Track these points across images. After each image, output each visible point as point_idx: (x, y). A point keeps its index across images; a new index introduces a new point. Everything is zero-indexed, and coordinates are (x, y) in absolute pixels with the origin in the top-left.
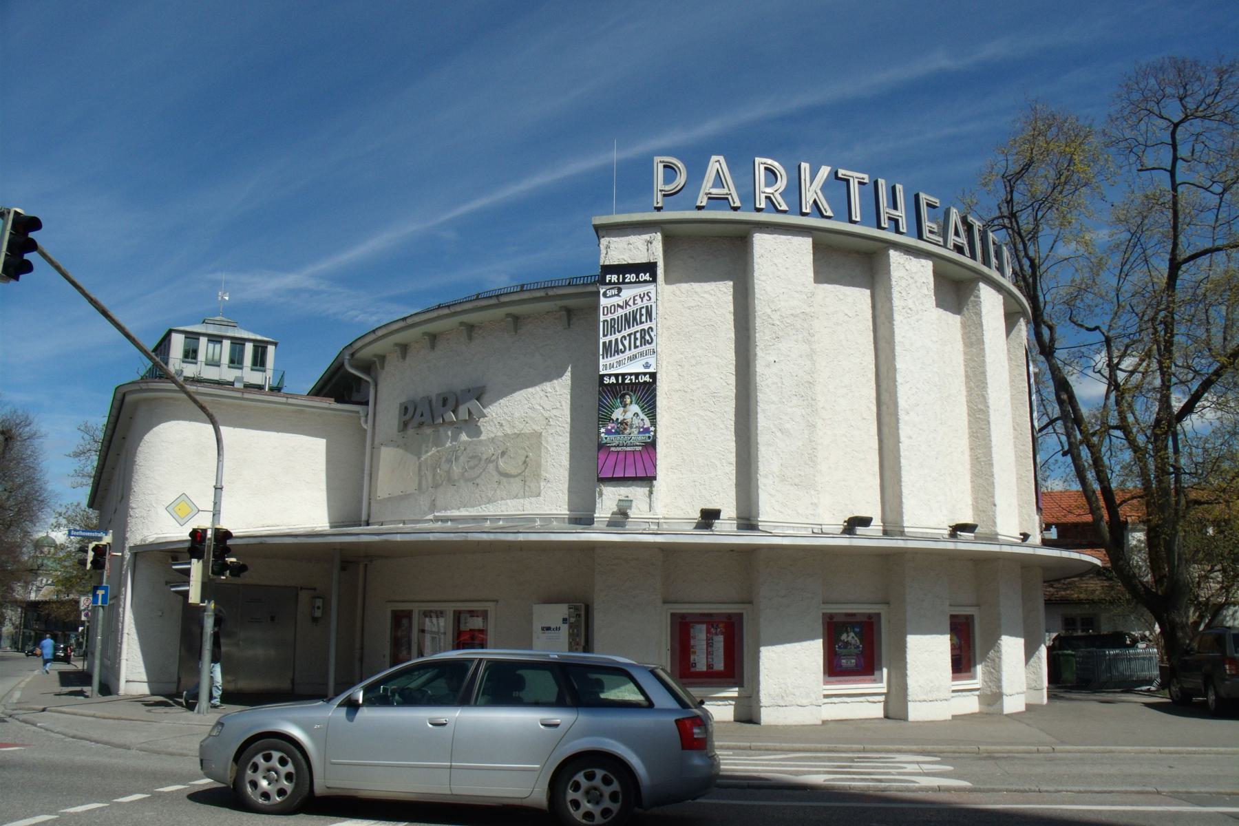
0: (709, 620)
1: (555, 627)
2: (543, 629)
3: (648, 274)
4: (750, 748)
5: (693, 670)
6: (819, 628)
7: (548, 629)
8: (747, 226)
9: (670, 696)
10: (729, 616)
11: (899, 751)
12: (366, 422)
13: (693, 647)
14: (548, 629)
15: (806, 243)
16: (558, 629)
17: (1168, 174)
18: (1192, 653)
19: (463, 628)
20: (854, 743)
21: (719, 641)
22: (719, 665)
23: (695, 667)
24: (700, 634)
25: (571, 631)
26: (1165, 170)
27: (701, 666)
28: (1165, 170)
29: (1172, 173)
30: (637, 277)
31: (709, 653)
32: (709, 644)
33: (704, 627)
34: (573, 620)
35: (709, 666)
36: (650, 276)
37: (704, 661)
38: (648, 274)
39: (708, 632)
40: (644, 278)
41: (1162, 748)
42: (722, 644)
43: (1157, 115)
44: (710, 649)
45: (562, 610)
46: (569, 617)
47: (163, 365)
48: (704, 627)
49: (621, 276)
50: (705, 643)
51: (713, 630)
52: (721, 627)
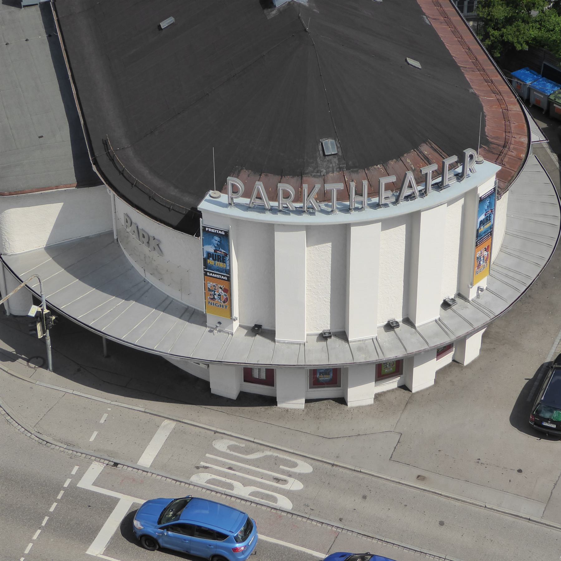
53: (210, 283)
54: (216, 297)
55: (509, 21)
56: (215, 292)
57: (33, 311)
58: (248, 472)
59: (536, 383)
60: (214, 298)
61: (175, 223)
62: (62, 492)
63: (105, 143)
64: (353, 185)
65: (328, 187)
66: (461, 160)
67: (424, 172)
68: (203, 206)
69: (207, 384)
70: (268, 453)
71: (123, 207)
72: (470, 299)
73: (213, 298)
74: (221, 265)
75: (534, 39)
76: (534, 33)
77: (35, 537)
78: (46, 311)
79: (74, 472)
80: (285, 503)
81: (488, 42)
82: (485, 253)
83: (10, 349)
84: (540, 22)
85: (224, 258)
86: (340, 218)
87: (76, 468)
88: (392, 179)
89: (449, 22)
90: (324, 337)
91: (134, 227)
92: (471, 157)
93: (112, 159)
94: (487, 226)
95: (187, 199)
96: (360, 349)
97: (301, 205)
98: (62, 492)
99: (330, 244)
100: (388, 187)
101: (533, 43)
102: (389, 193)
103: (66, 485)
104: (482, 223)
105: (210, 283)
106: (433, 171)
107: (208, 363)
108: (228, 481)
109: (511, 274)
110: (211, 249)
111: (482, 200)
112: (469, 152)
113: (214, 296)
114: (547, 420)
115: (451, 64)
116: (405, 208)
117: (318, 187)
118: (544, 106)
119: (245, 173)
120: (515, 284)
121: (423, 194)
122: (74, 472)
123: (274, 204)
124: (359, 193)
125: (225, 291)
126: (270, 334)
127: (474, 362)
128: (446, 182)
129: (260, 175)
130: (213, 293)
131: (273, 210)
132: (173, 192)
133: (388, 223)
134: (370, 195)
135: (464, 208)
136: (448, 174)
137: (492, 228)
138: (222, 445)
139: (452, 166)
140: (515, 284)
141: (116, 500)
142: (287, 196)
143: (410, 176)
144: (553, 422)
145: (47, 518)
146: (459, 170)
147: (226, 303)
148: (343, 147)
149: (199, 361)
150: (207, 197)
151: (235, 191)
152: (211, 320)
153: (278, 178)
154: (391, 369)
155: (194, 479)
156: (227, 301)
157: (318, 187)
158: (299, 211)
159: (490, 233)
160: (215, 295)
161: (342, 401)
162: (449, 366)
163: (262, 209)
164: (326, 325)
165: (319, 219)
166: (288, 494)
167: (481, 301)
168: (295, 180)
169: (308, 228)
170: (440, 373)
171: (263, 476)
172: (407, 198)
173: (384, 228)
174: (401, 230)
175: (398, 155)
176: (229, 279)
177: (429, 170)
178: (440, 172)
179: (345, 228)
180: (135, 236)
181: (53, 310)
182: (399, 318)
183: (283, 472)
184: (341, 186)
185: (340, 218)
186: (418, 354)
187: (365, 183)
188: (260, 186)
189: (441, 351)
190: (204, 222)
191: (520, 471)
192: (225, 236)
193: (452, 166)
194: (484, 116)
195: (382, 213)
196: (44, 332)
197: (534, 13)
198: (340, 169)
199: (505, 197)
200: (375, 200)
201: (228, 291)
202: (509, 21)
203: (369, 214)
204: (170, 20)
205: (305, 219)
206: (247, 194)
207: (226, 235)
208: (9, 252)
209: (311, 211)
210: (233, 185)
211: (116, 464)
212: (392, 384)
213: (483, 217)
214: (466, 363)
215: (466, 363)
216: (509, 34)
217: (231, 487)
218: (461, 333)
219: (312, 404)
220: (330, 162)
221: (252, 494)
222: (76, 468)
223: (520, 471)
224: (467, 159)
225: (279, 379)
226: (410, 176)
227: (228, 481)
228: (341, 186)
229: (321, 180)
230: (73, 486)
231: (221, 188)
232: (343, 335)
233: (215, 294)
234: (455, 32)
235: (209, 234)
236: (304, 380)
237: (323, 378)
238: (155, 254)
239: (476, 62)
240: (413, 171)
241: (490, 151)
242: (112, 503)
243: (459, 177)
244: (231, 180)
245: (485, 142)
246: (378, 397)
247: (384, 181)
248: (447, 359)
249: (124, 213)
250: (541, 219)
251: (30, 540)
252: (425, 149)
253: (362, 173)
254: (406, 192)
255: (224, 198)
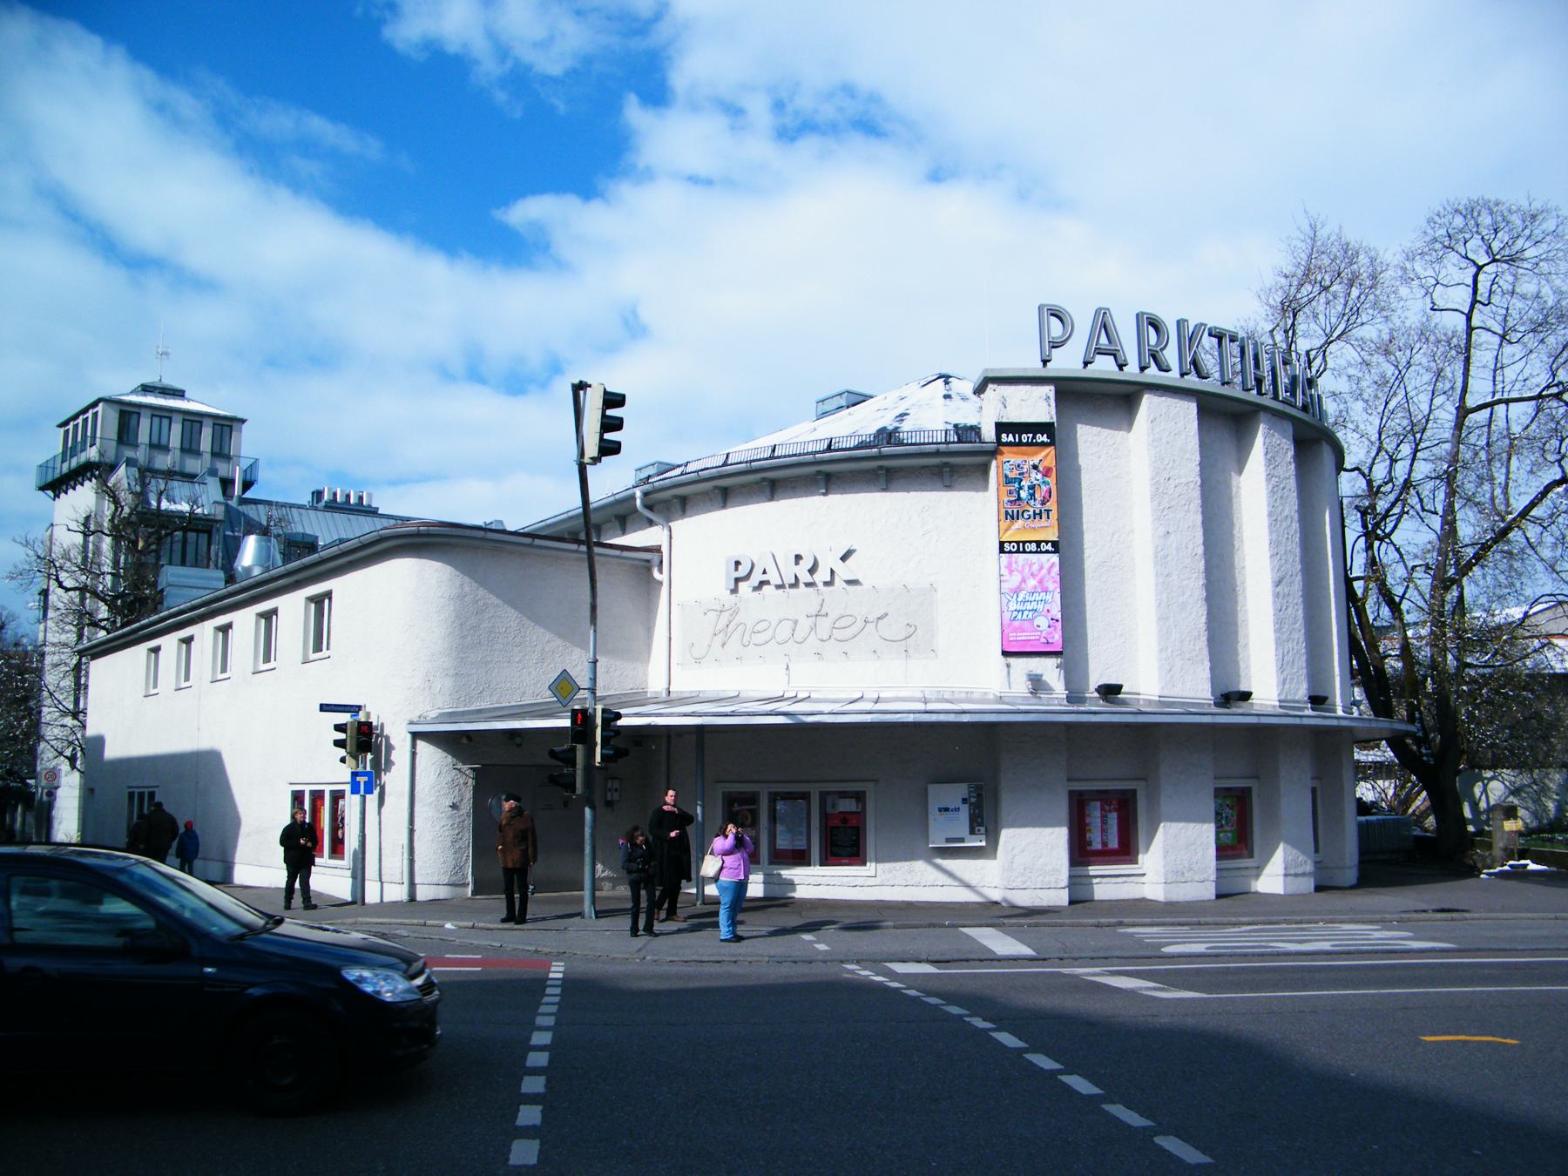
0: (1103, 796)
1: (953, 807)
2: (940, 810)
3: (1045, 435)
4: (1199, 924)
5: (1088, 848)
6: (1210, 806)
7: (946, 810)
8: (1135, 387)
9: (1421, 886)
10: (1124, 792)
11: (1342, 922)
12: (661, 571)
13: (1088, 825)
14: (946, 810)
15: (1191, 407)
16: (957, 810)
17: (1464, 317)
18: (1374, 810)
19: (829, 810)
20: (1243, 916)
21: (1113, 818)
22: (1114, 844)
23: (1091, 845)
24: (1094, 814)
25: (972, 811)
26: (1463, 313)
27: (1097, 845)
28: (1463, 313)
29: (1469, 318)
30: (1034, 437)
31: (1104, 831)
32: (1104, 822)
33: (1098, 804)
34: (973, 800)
35: (1104, 844)
36: (1048, 438)
37: (1099, 839)
38: (1045, 435)
39: (1102, 809)
40: (1042, 439)
41: (1558, 915)
42: (1115, 822)
43: (1461, 255)
44: (1104, 827)
45: (962, 790)
46: (970, 797)
47: (88, 445)
48: (1098, 804)
49: (1017, 435)
50: (1099, 820)
51: (1107, 808)
52: (1115, 805)
53: (1008, 462)
54: (1024, 494)
56: (1022, 480)
60: (1019, 498)
73: (1015, 500)
99: (1079, 426)
101: (1474, 709)
105: (1008, 462)
106: (321, 651)
113: (1019, 495)
130: (1016, 485)
147: (1048, 504)
154: (1417, 568)
156: (1050, 497)
160: (1021, 491)
233: (1021, 488)
249: (590, 386)
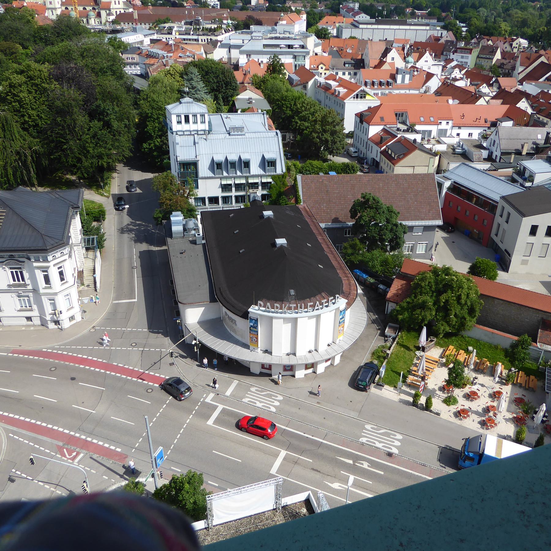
55: (352, 254)
57: (194, 342)
58: (260, 398)
59: (358, 372)
61: (240, 315)
62: (200, 403)
63: (220, 288)
64: (299, 305)
65: (291, 305)
66: (335, 298)
67: (322, 301)
68: (250, 310)
69: (249, 369)
70: (268, 392)
71: (224, 309)
72: (337, 343)
74: (255, 329)
75: (360, 260)
76: (360, 258)
77: (190, 417)
78: (198, 343)
79: (204, 396)
80: (273, 409)
81: (346, 260)
82: (342, 328)
83: (185, 355)
84: (363, 255)
85: (256, 327)
86: (294, 315)
87: (205, 395)
88: (312, 304)
89: (332, 254)
90: (288, 355)
91: (228, 316)
92: (338, 297)
93: (222, 294)
94: (343, 319)
95: (245, 307)
96: (300, 359)
97: (282, 311)
98: (200, 403)
100: (310, 306)
102: (311, 308)
103: (201, 400)
104: (341, 319)
107: (250, 362)
108: (255, 401)
109: (350, 336)
110: (252, 324)
111: (341, 312)
112: (337, 296)
114: (360, 385)
115: (333, 267)
116: (316, 313)
117: (287, 305)
118: (363, 281)
119: (264, 300)
120: (351, 339)
121: (322, 309)
122: (204, 396)
123: (273, 310)
124: (301, 308)
125: (256, 338)
126: (271, 353)
127: (338, 365)
128: (329, 305)
129: (41, 132)
131: (272, 312)
132: (241, 305)
133: (310, 317)
134: (304, 308)
135: (335, 313)
136: (330, 303)
137: (344, 320)
138: (253, 389)
139: (331, 300)
140: (351, 339)
141: (217, 407)
142: (277, 308)
143: (318, 303)
144: (362, 386)
145: (194, 411)
146: (334, 301)
148: (296, 292)
149: (247, 361)
150: (251, 307)
151: (261, 305)
152: (251, 348)
153: (275, 302)
154: (310, 366)
155: (243, 400)
157: (287, 305)
158: (281, 313)
159: (344, 321)
161: (294, 376)
162: (329, 366)
163: (269, 312)
164: (288, 351)
165: (287, 315)
166: (274, 406)
167: (340, 344)
168: (280, 303)
169: (284, 319)
170: (326, 368)
171: (266, 400)
172: (316, 310)
173: (308, 319)
174: (314, 320)
175: (314, 296)
176: (257, 334)
177: (324, 301)
178: (328, 302)
179: (296, 319)
180: (228, 319)
181: (200, 342)
182: (313, 349)
183: (273, 399)
184: (295, 305)
185: (294, 315)
186: (319, 361)
187: (303, 305)
188: (268, 304)
189: (327, 361)
190: (250, 315)
191: (351, 402)
192: (257, 320)
193: (331, 300)
194: (343, 284)
195: (308, 314)
196: (197, 349)
197: (361, 252)
198: (295, 300)
199: (349, 310)
200: (306, 310)
201: (257, 338)
202: (352, 254)
203: (304, 314)
204: (243, 250)
205: (283, 315)
206: (264, 307)
207: (257, 319)
208: (187, 323)
209: (285, 313)
210: (260, 304)
211: (218, 394)
212: (310, 371)
213: (341, 317)
214: (335, 364)
215: (335, 364)
216: (352, 258)
217: (256, 403)
218: (333, 355)
219: (284, 377)
220: (292, 297)
221: (263, 406)
222: (205, 395)
223: (351, 402)
224: (337, 298)
225: (273, 368)
226: (318, 303)
227: (255, 401)
228: (295, 305)
229: (289, 303)
230: (204, 401)
231: (256, 304)
232: (294, 354)
234: (335, 257)
235: (251, 320)
236: (281, 370)
237: (308, 367)
238: (234, 325)
239: (341, 267)
240: (319, 301)
241: (344, 296)
242: (216, 407)
243: (334, 303)
244: (259, 302)
245: (343, 292)
246: (305, 375)
247: (309, 304)
248: (329, 363)
250: (361, 318)
251: (188, 418)
252: (323, 294)
253: (302, 301)
254: (316, 308)
255: (257, 308)
